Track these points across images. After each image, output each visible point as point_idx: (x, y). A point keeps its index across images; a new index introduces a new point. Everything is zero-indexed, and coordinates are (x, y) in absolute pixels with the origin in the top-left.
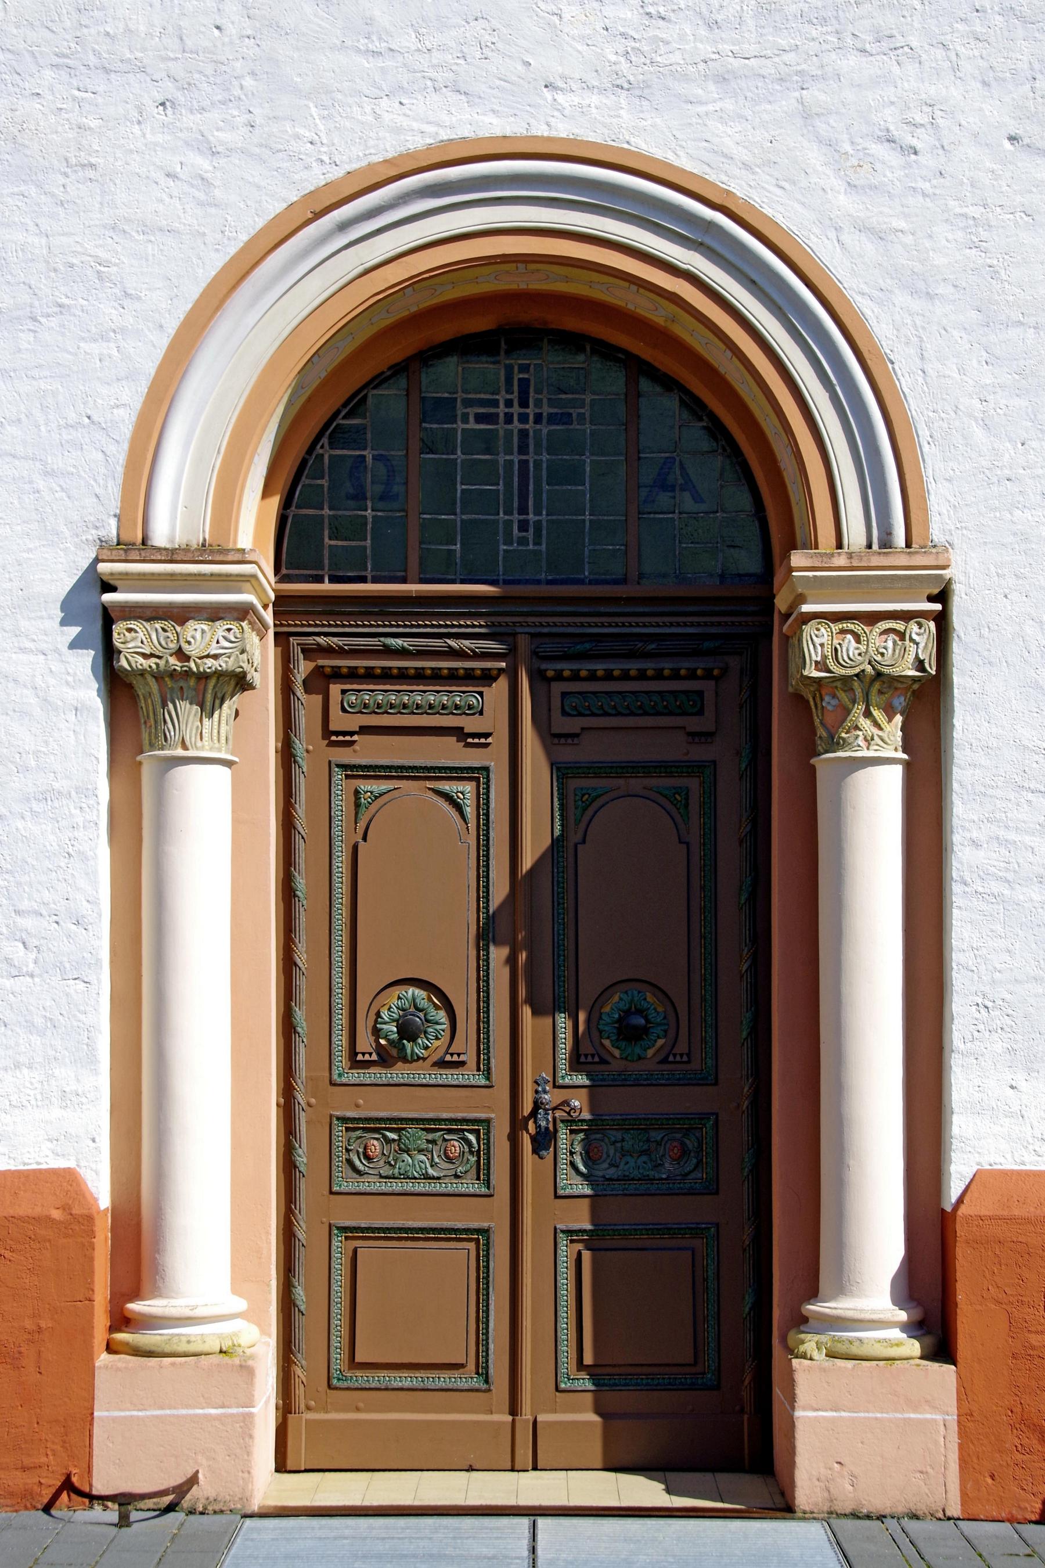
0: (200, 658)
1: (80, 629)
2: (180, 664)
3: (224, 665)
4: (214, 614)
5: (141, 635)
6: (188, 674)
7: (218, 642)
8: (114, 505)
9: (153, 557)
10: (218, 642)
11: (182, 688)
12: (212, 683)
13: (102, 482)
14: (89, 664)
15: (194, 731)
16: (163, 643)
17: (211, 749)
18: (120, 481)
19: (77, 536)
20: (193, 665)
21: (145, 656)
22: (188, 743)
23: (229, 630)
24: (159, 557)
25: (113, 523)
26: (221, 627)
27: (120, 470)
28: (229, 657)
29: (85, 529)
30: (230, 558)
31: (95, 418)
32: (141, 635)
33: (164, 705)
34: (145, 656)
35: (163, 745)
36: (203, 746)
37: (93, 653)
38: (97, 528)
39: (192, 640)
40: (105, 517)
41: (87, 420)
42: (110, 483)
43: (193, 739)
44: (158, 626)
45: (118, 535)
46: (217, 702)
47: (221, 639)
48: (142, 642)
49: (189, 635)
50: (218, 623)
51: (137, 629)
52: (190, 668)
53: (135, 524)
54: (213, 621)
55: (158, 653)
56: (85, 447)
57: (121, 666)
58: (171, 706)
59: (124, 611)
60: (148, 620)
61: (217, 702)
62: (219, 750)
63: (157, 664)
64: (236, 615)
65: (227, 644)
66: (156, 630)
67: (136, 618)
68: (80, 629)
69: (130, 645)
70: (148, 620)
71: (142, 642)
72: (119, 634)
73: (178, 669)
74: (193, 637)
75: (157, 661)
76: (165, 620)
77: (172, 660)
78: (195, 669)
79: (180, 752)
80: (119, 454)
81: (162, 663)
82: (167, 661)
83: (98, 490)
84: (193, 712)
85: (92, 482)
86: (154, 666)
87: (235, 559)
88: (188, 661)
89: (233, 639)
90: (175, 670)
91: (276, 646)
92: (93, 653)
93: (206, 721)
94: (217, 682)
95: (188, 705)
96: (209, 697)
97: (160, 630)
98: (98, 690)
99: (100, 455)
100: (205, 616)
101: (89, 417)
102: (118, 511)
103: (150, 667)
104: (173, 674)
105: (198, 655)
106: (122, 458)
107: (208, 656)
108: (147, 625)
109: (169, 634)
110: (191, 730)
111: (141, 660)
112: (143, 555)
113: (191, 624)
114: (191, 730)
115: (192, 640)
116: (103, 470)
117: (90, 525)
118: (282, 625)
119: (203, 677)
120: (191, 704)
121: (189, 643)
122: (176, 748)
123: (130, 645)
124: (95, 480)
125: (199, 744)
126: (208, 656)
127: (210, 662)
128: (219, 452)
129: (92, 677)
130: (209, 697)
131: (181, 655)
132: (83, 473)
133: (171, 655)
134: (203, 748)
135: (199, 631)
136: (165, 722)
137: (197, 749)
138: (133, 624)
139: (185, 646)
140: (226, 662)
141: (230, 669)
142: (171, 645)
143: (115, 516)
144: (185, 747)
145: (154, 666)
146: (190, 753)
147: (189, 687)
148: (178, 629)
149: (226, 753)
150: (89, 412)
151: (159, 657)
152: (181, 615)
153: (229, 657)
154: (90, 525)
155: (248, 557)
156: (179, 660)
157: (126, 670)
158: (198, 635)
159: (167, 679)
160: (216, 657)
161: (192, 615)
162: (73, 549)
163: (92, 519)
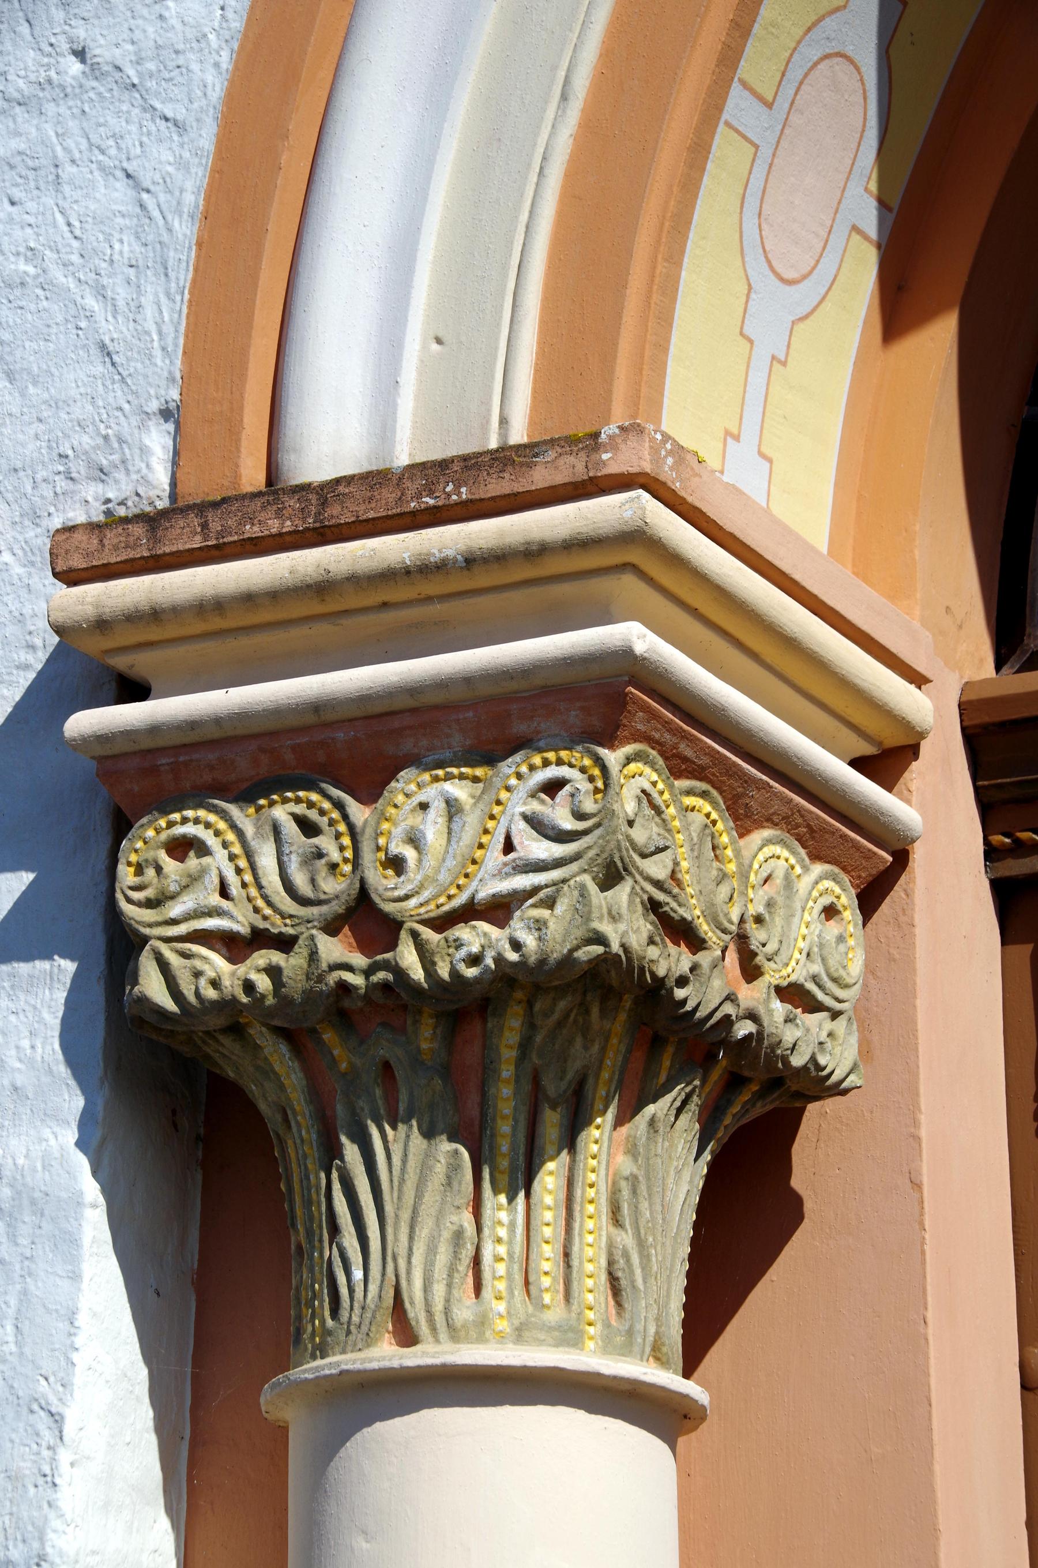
0: (443, 923)
1: (27, 877)
2: (359, 960)
3: (530, 941)
4: (487, 726)
5: (219, 859)
6: (396, 996)
7: (509, 847)
8: (159, 372)
9: (251, 531)
10: (509, 847)
11: (387, 1066)
12: (510, 1032)
13: (122, 294)
14: (53, 1019)
15: (443, 1257)
16: (300, 880)
17: (520, 1334)
18: (183, 276)
19: (35, 518)
20: (408, 957)
21: (234, 946)
22: (416, 1312)
23: (552, 788)
24: (274, 526)
25: (158, 441)
26: (520, 778)
27: (185, 230)
28: (550, 903)
29: (62, 484)
30: (541, 477)
31: (102, 51)
32: (219, 859)
33: (332, 1152)
34: (234, 946)
35: (327, 1332)
36: (482, 1322)
37: (69, 967)
38: (102, 474)
39: (410, 854)
40: (127, 427)
41: (75, 67)
42: (152, 289)
43: (439, 1290)
44: (280, 813)
45: (173, 484)
46: (552, 1121)
47: (520, 827)
48: (224, 892)
49: (398, 831)
50: (507, 767)
51: (211, 841)
52: (400, 973)
53: (234, 431)
54: (491, 760)
55: (278, 926)
56: (68, 170)
57: (143, 1001)
58: (351, 1152)
59: (153, 771)
60: (248, 794)
61: (552, 1121)
62: (570, 1335)
63: (273, 972)
64: (574, 717)
65: (543, 849)
66: (276, 830)
67: (200, 794)
68: (27, 877)
69: (175, 910)
70: (246, 796)
71: (224, 892)
72: (139, 870)
73: (357, 980)
74: (414, 840)
75: (276, 957)
76: (311, 785)
77: (333, 949)
78: (418, 974)
79: (385, 1354)
80: (181, 169)
81: (292, 963)
82: (313, 956)
83: (109, 328)
84: (440, 1169)
85: (91, 302)
86: (263, 983)
87: (560, 477)
88: (392, 945)
89: (568, 824)
90: (343, 987)
91: (1006, 939)
92: (69, 967)
93: (495, 1204)
94: (531, 1026)
95: (417, 1141)
96: (506, 1098)
97: (290, 829)
98: (85, 1122)
99: (121, 192)
100: (458, 741)
101: (80, 54)
102: (174, 394)
103: (249, 987)
104: (339, 1005)
105: (431, 911)
106: (192, 188)
107: (469, 913)
108: (243, 817)
109: (325, 842)
110: (432, 1250)
111: (216, 963)
112: (215, 526)
113: (409, 786)
114: (432, 1250)
115: (410, 854)
116: (127, 248)
117: (78, 468)
118: (1020, 849)
119: (467, 1006)
120: (429, 1134)
121: (396, 864)
122: (369, 1341)
123: (175, 910)
124: (101, 293)
125: (465, 1311)
126: (469, 913)
127: (473, 936)
128: (564, 97)
129: (62, 1070)
130: (506, 1098)
131: (367, 920)
132: (58, 275)
133: (332, 928)
134: (480, 1329)
135: (438, 807)
136: (335, 1230)
137: (455, 1333)
138: (193, 822)
139: (383, 883)
140: (539, 925)
141: (558, 951)
142: (331, 886)
143: (166, 414)
144: (406, 1335)
145: (263, 983)
146: (429, 1353)
147: (416, 1061)
148: (359, 813)
149: (608, 1347)
150: (81, 32)
151: (285, 944)
152: (352, 755)
153: (550, 903)
154: (78, 468)
155: (613, 462)
156: (365, 946)
157: (160, 1012)
158: (433, 827)
159: (328, 1036)
160: (499, 910)
161: (408, 745)
162: (18, 570)
163: (86, 441)
